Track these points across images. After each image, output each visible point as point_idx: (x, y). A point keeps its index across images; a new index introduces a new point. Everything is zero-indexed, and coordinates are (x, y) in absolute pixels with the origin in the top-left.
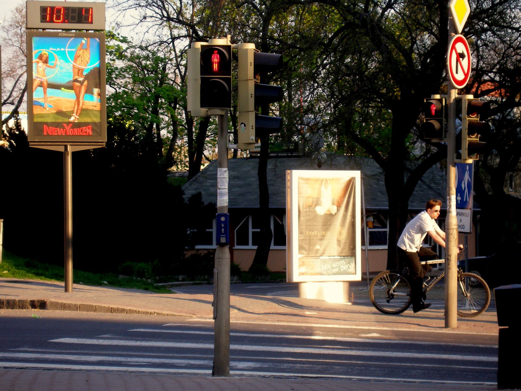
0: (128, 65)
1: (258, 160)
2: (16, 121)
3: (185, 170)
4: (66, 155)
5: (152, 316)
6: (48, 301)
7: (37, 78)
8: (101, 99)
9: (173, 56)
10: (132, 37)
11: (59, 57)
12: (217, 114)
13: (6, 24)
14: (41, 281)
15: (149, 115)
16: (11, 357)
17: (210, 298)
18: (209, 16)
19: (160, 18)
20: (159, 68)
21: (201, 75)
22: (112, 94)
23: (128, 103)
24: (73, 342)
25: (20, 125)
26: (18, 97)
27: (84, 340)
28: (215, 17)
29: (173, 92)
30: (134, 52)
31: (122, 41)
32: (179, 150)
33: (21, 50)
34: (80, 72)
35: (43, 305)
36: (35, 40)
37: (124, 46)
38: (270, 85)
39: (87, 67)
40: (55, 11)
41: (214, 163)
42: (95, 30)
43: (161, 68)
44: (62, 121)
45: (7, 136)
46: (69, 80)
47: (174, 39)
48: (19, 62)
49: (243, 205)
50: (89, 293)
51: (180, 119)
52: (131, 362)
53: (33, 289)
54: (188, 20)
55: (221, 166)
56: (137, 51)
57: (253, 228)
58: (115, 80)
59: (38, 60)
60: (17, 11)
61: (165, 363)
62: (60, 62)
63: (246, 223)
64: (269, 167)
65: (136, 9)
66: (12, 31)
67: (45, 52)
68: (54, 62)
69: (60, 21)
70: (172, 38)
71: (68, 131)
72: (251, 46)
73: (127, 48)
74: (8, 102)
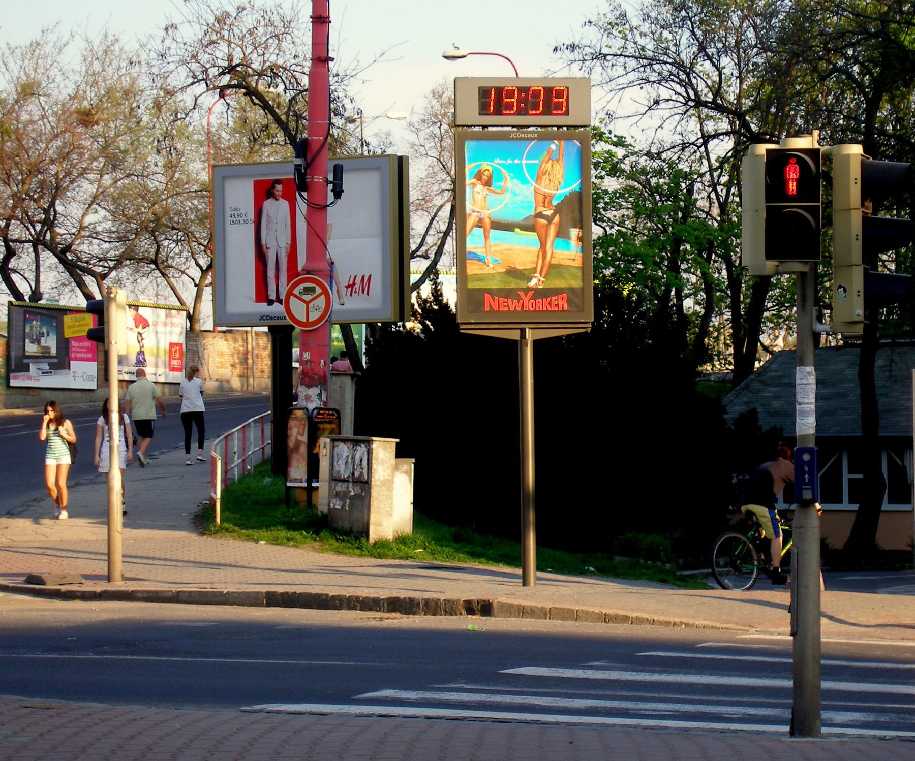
0: (627, 186)
1: (857, 351)
2: (433, 286)
3: (727, 369)
4: (524, 346)
5: (677, 629)
6: (496, 601)
7: (473, 211)
8: (582, 247)
9: (705, 168)
10: (632, 137)
11: (512, 175)
12: (797, 270)
13: (416, 119)
14: (481, 567)
15: (663, 273)
16: (436, 699)
17: (784, 597)
18: (769, 97)
19: (684, 101)
20: (682, 191)
21: (766, 202)
22: (599, 238)
23: (628, 253)
24: (411, 708)
25: (441, 295)
26: (435, 244)
27: (561, 670)
28: (781, 98)
29: (706, 232)
30: (637, 162)
31: (616, 145)
32: (716, 334)
33: (441, 163)
34: (547, 200)
35: (486, 609)
36: (469, 146)
37: (620, 152)
38: (879, 216)
39: (560, 191)
40: (531, 95)
41: (779, 356)
42: (568, 127)
43: (685, 191)
44: (517, 287)
45: (419, 314)
46: (528, 215)
47: (707, 138)
48: (437, 185)
49: (831, 431)
50: (565, 588)
51: (718, 279)
52: (644, 710)
53: (467, 581)
54: (730, 103)
55: (802, 363)
56: (643, 161)
57: (850, 472)
58: (603, 213)
59: (474, 181)
60: (433, 96)
61: (705, 713)
62: (512, 184)
63: (838, 466)
64: (879, 363)
65: (642, 88)
66: (425, 132)
67: (486, 165)
68: (502, 184)
69: (512, 112)
70: (703, 136)
71: (526, 304)
72: (856, 150)
73: (625, 157)
74: (418, 253)
